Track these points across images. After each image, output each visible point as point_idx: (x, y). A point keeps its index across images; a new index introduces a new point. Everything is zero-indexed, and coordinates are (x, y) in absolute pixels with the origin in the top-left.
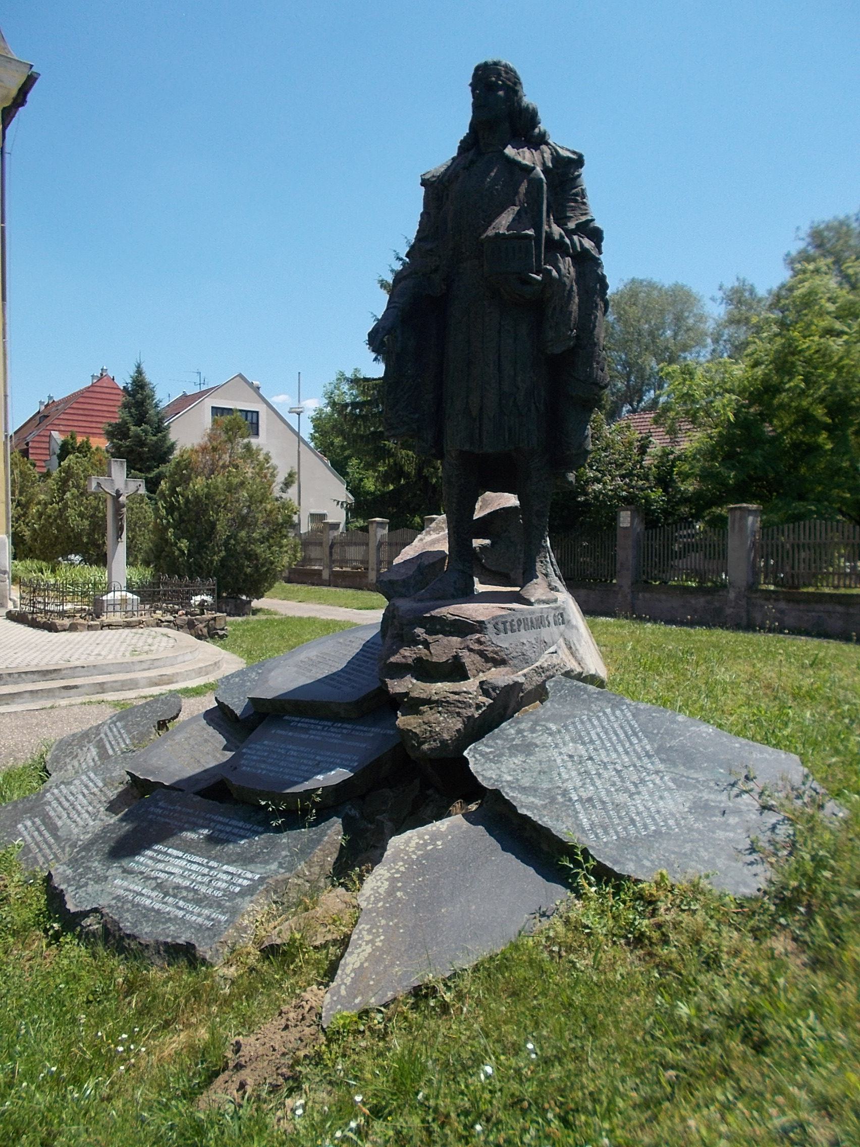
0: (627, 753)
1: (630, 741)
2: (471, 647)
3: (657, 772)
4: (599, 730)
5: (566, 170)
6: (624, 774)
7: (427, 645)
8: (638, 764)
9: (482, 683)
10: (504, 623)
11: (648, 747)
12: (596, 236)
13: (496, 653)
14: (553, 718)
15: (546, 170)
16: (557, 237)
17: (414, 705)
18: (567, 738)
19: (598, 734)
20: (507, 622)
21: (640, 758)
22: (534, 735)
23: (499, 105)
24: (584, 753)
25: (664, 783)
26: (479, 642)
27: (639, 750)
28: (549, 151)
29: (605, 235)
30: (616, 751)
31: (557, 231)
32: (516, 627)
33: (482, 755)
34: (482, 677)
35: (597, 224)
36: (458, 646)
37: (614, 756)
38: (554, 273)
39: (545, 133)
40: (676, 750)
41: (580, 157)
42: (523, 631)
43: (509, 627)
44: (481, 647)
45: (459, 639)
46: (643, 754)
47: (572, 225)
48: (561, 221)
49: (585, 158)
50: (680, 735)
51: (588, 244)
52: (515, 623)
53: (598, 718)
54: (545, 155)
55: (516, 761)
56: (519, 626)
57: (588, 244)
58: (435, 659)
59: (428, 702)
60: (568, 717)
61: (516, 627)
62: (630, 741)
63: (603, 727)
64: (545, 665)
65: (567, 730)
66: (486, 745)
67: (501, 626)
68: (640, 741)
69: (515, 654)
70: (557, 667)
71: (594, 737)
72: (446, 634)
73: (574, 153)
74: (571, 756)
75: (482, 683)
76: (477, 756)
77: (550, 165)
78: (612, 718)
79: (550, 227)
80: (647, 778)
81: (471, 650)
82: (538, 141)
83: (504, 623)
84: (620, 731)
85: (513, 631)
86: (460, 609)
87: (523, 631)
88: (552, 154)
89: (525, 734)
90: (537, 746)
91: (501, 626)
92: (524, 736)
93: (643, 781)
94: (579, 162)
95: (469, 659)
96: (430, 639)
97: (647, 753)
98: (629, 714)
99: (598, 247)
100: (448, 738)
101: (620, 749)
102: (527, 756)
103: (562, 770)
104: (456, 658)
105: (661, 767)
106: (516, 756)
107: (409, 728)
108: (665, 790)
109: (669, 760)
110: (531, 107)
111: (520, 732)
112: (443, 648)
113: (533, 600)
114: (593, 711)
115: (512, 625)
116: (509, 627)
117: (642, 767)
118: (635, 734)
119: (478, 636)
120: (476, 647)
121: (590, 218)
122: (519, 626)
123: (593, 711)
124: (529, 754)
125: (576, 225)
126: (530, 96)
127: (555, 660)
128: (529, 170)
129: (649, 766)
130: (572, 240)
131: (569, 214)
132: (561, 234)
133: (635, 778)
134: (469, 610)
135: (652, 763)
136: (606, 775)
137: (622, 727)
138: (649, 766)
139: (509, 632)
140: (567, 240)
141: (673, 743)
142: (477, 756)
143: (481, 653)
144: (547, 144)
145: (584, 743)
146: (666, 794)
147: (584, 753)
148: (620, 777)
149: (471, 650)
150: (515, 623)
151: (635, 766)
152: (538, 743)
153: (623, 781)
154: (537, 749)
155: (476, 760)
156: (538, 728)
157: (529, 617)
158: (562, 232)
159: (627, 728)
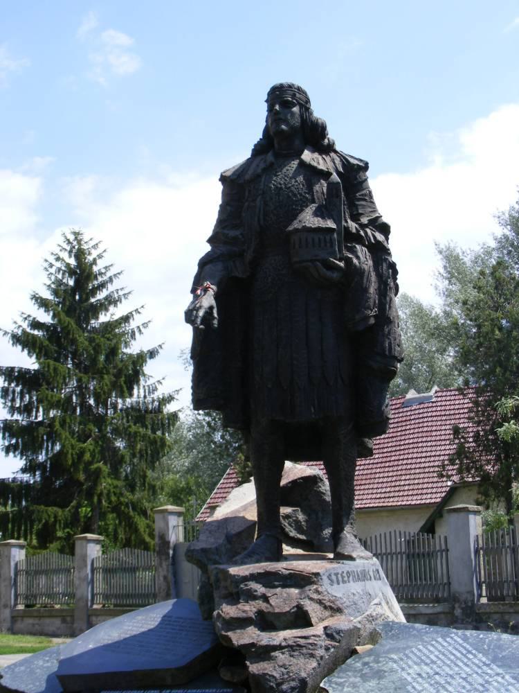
0: (468, 666)
1: (467, 657)
2: (311, 596)
3: (498, 674)
4: (437, 653)
5: (354, 174)
6: (469, 679)
7: (265, 598)
8: (480, 671)
9: (325, 628)
10: (336, 574)
11: (484, 659)
12: (385, 229)
13: (332, 602)
14: (397, 650)
15: (339, 173)
16: (354, 231)
17: (265, 653)
18: (410, 663)
19: (437, 657)
20: (338, 574)
21: (479, 667)
22: (380, 665)
23: (291, 125)
24: (429, 670)
25: (506, 680)
26: (317, 591)
27: (477, 662)
28: (339, 159)
29: (391, 230)
30: (457, 666)
31: (353, 226)
32: (346, 579)
33: (336, 684)
34: (326, 623)
35: (385, 219)
36: (298, 596)
37: (457, 669)
38: (355, 261)
39: (334, 144)
40: (508, 658)
41: (367, 164)
42: (351, 582)
43: (340, 579)
44: (320, 597)
45: (297, 591)
46: (481, 664)
47: (365, 220)
48: (356, 218)
49: (369, 165)
50: (508, 648)
51: (380, 237)
52: (345, 575)
53: (433, 645)
54: (336, 162)
55: (371, 684)
56: (348, 577)
57: (380, 237)
58: (277, 610)
59: (279, 648)
60: (405, 649)
61: (346, 579)
62: (467, 657)
63: (440, 651)
64: (374, 614)
65: (408, 657)
66: (338, 677)
67: (334, 577)
68: (475, 656)
69: (348, 603)
70: (383, 617)
71: (435, 659)
72: (284, 586)
73: (361, 161)
74: (419, 675)
75: (325, 628)
76: (334, 685)
77: (341, 170)
78: (445, 644)
79: (347, 222)
80: (490, 680)
81: (311, 599)
82: (327, 149)
83: (336, 574)
84: (454, 652)
85: (344, 582)
86: (292, 564)
87: (351, 582)
88: (341, 160)
89: (371, 665)
90: (385, 672)
91: (334, 577)
92: (371, 667)
93: (487, 682)
94: (366, 167)
95: (312, 609)
96: (269, 592)
97: (485, 664)
98: (459, 640)
99: (387, 239)
100: (306, 676)
101: (461, 664)
102: (379, 679)
103: (414, 684)
104: (299, 607)
105: (500, 671)
106: (370, 681)
107: (266, 672)
108: (508, 685)
109: (505, 665)
110: (320, 121)
111: (366, 664)
112: (283, 599)
113: (354, 555)
114: (426, 642)
115: (343, 577)
116: (340, 579)
117: (484, 673)
118: (469, 652)
119: (315, 587)
120: (315, 596)
121: (377, 215)
122: (348, 577)
123: (426, 642)
124: (380, 678)
125: (369, 220)
126: (319, 111)
127: (379, 610)
128: (326, 175)
129: (489, 671)
130: (366, 233)
131: (360, 211)
132: (356, 228)
133: (480, 680)
134: (301, 565)
135: (492, 669)
136: (454, 682)
137: (456, 649)
138: (489, 671)
139: (341, 583)
140: (362, 233)
141: (504, 654)
142: (334, 685)
143: (320, 602)
144: (336, 152)
145: (426, 664)
146: (510, 687)
147: (429, 670)
148: (467, 682)
149: (311, 599)
150: (345, 575)
151: (477, 673)
152: (385, 669)
153: (471, 684)
154: (386, 674)
155: (333, 688)
156: (381, 659)
157: (355, 570)
158: (357, 226)
159: (461, 649)
